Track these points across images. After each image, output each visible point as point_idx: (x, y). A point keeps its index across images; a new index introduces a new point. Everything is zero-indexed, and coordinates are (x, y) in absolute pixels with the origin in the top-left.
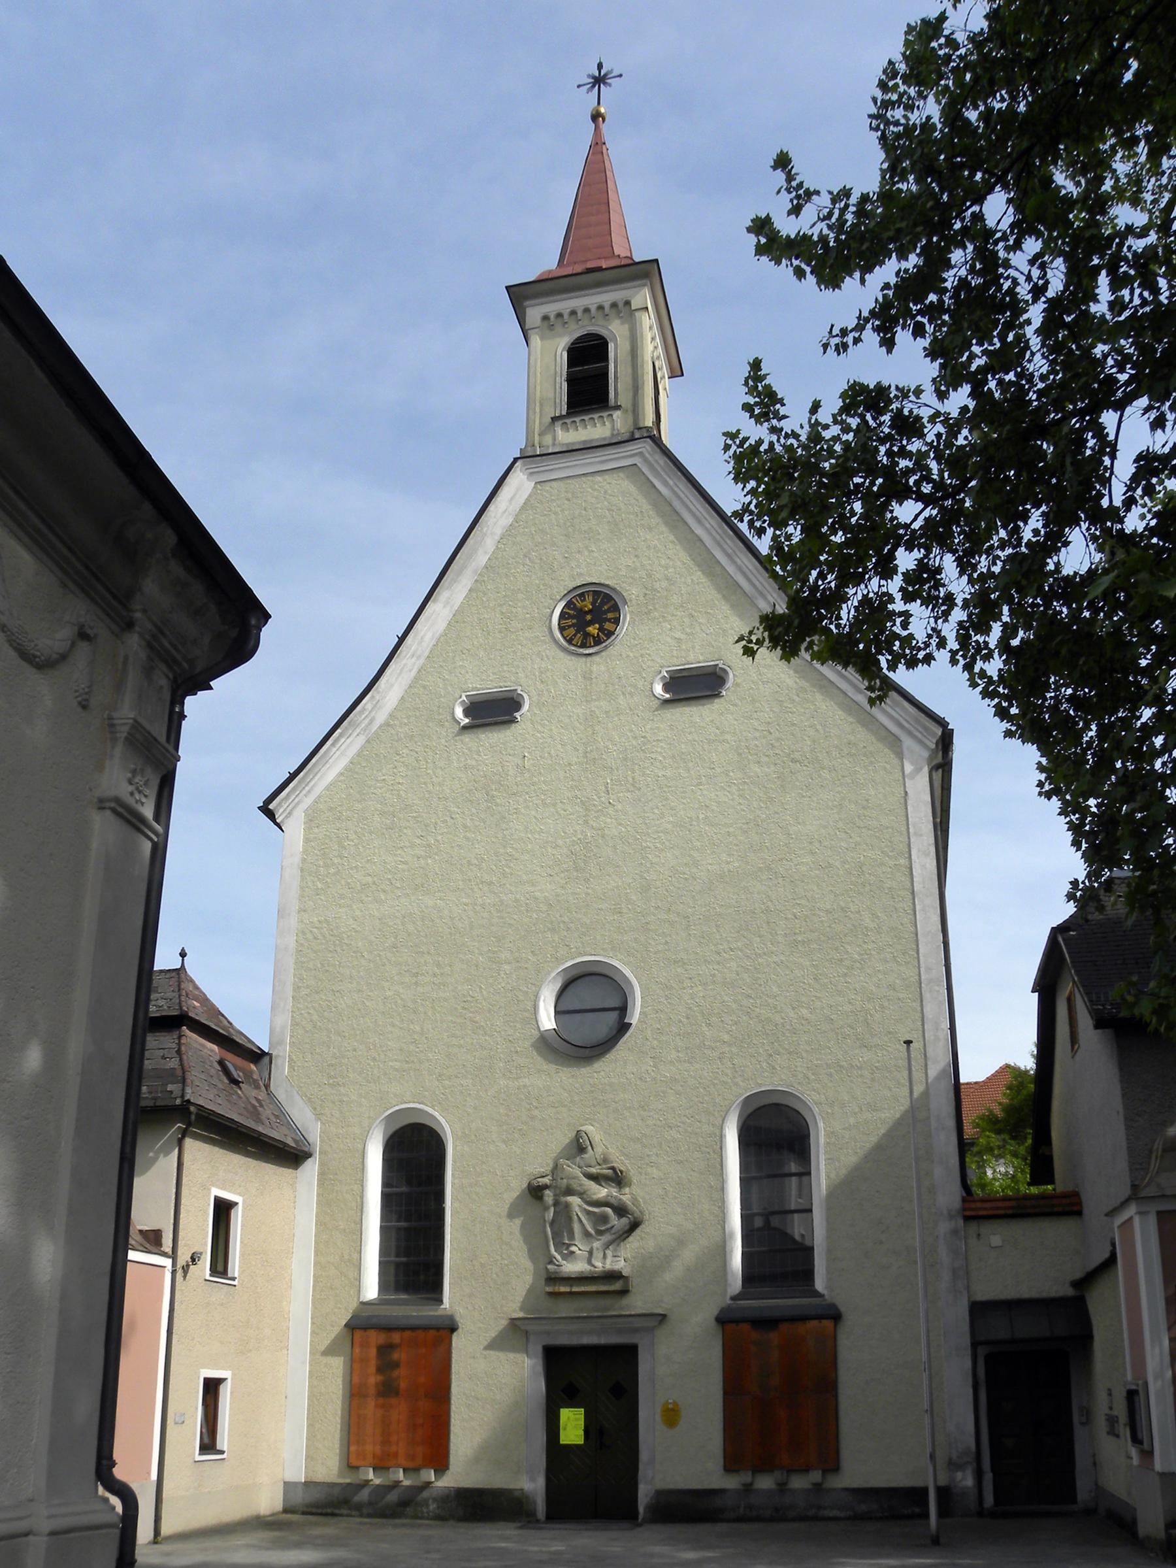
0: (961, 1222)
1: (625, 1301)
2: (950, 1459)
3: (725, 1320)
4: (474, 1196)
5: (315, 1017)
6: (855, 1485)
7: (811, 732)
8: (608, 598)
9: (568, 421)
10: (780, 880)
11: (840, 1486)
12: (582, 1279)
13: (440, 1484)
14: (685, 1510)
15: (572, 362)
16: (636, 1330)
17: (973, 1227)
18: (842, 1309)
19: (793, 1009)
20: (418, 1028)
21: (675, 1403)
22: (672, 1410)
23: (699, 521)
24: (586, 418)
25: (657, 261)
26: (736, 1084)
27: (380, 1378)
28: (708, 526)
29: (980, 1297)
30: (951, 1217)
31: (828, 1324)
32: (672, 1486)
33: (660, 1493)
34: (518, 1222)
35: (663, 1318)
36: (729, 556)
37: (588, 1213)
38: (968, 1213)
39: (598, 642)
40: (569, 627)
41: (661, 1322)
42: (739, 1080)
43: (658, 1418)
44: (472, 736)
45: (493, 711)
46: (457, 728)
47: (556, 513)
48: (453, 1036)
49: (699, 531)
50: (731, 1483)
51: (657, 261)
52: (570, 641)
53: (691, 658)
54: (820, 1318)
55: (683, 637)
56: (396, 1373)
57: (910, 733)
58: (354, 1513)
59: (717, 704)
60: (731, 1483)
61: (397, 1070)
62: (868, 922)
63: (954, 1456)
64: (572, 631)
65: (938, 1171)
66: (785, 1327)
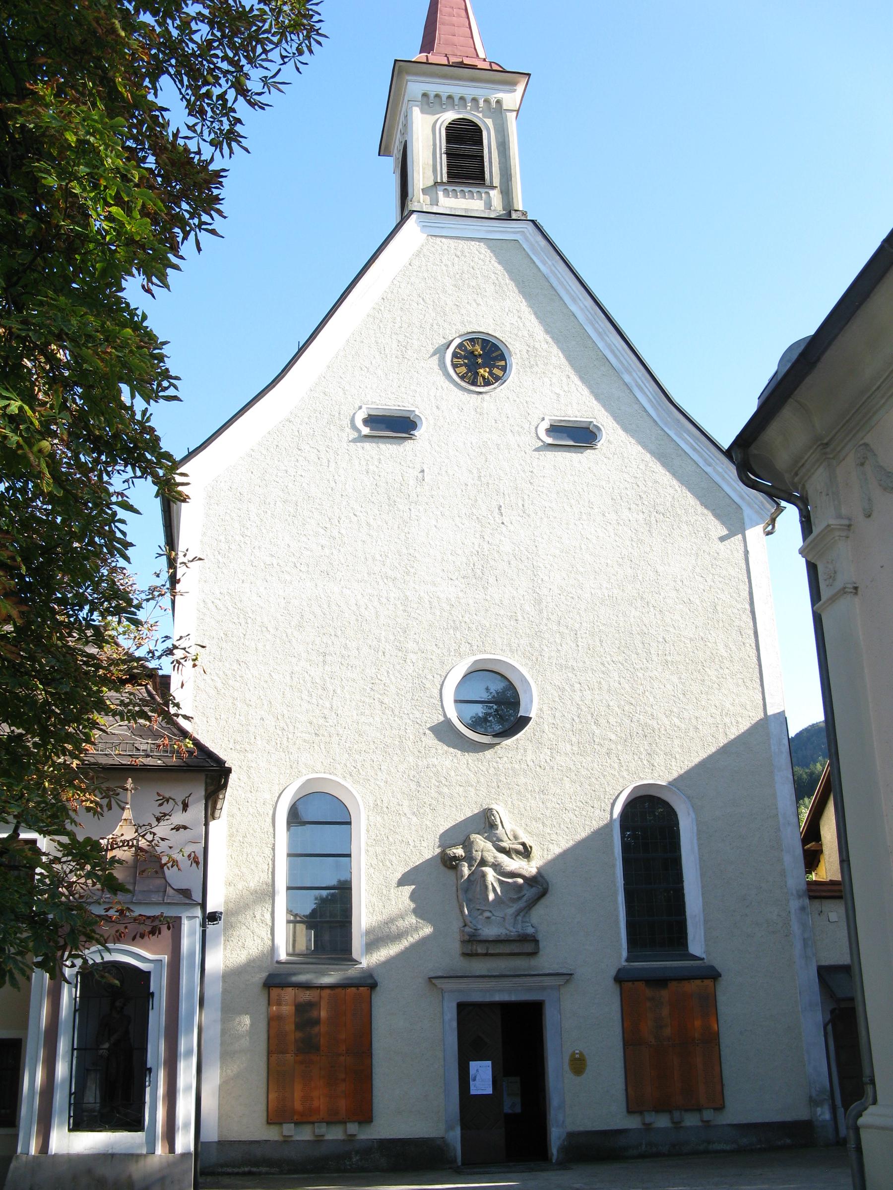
0: (807, 901)
1: (534, 962)
2: (811, 1097)
3: (620, 978)
4: (388, 863)
5: (219, 685)
6: (744, 1121)
7: (672, 491)
8: (495, 347)
9: (450, 188)
10: (652, 609)
11: (725, 1123)
12: (498, 941)
13: (362, 1136)
14: (595, 1150)
15: (449, 140)
16: (543, 988)
17: (816, 903)
18: (379, 980)
19: (667, 717)
20: (328, 705)
21: (581, 1054)
22: (579, 1059)
23: (574, 300)
24: (466, 189)
25: (396, 61)
26: (623, 777)
27: (299, 1035)
28: (581, 305)
29: (823, 963)
30: (799, 897)
31: (708, 982)
32: (581, 1129)
33: (571, 1135)
34: (408, 889)
35: (568, 976)
36: (600, 334)
37: (499, 880)
38: (812, 894)
39: (487, 383)
40: (461, 365)
41: (567, 981)
42: (625, 774)
43: (566, 1067)
44: (374, 445)
45: (395, 426)
46: (356, 435)
47: (446, 265)
48: (362, 714)
49: (573, 308)
50: (633, 1123)
51: (396, 61)
52: (462, 378)
53: (570, 412)
54: (703, 978)
55: (562, 393)
56: (316, 1030)
57: (749, 505)
58: (273, 1170)
59: (408, 444)
60: (633, 1123)
61: (305, 741)
62: (723, 651)
63: (814, 1094)
64: (463, 370)
65: (787, 859)
66: (673, 985)
